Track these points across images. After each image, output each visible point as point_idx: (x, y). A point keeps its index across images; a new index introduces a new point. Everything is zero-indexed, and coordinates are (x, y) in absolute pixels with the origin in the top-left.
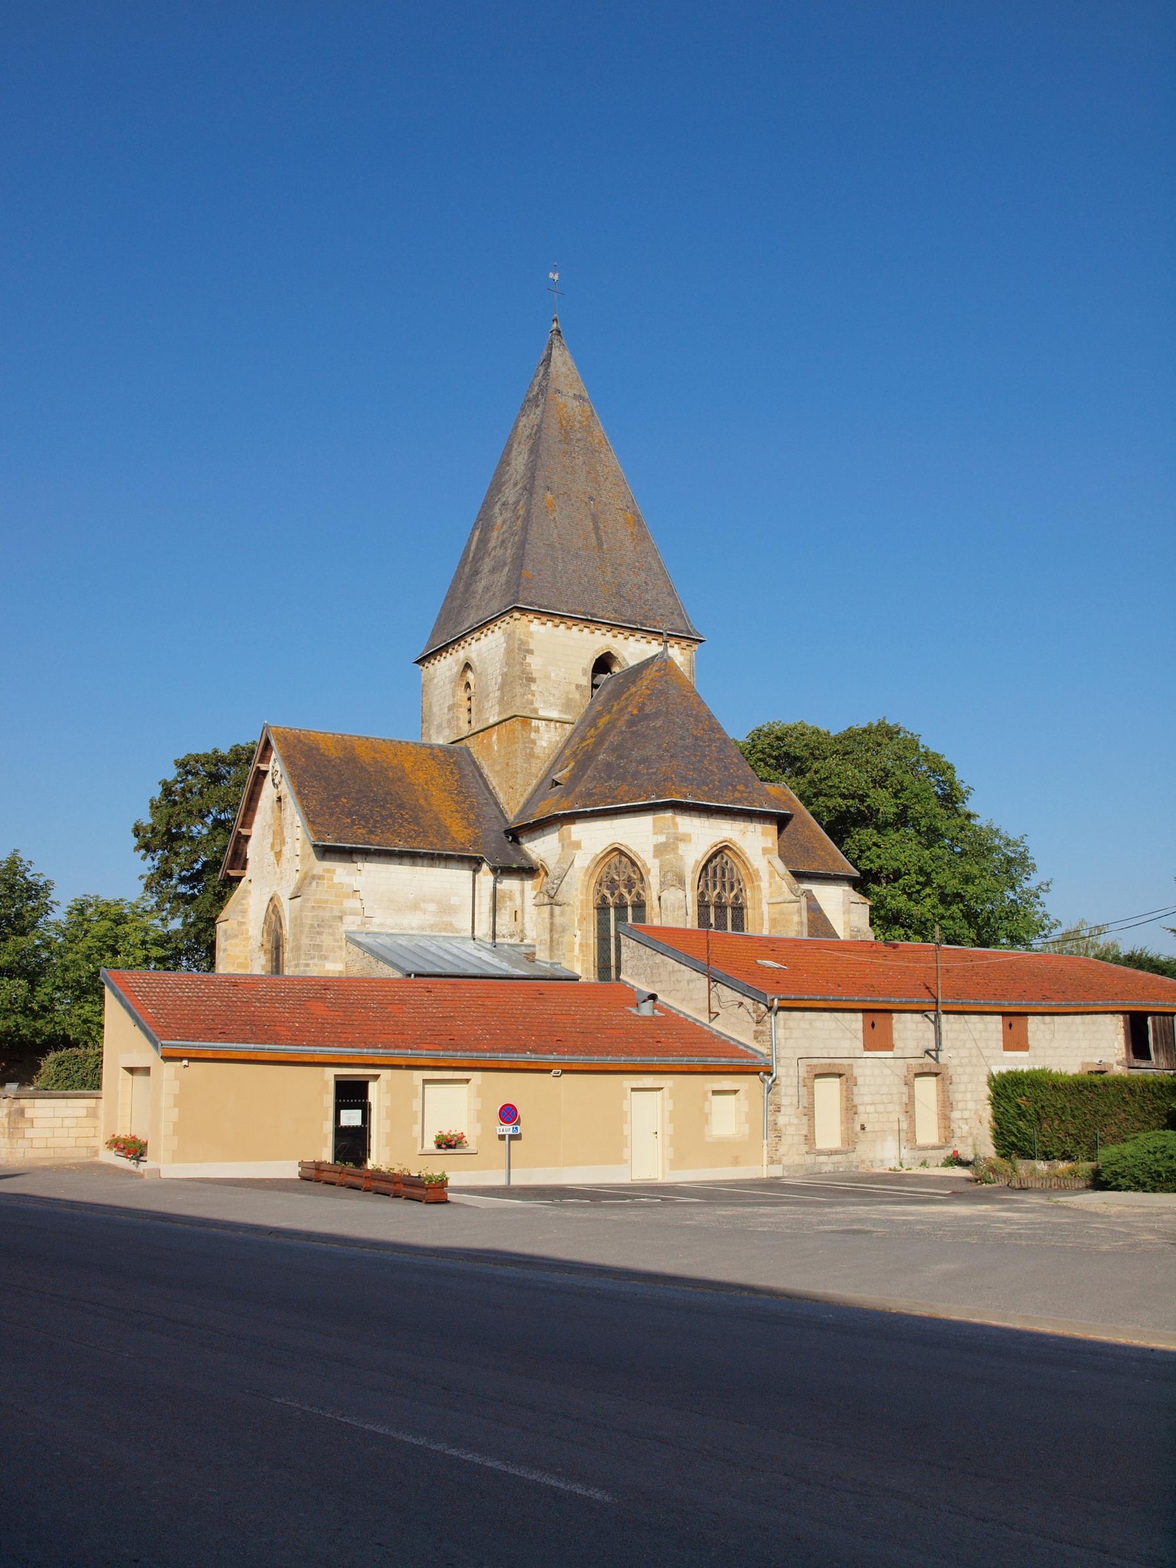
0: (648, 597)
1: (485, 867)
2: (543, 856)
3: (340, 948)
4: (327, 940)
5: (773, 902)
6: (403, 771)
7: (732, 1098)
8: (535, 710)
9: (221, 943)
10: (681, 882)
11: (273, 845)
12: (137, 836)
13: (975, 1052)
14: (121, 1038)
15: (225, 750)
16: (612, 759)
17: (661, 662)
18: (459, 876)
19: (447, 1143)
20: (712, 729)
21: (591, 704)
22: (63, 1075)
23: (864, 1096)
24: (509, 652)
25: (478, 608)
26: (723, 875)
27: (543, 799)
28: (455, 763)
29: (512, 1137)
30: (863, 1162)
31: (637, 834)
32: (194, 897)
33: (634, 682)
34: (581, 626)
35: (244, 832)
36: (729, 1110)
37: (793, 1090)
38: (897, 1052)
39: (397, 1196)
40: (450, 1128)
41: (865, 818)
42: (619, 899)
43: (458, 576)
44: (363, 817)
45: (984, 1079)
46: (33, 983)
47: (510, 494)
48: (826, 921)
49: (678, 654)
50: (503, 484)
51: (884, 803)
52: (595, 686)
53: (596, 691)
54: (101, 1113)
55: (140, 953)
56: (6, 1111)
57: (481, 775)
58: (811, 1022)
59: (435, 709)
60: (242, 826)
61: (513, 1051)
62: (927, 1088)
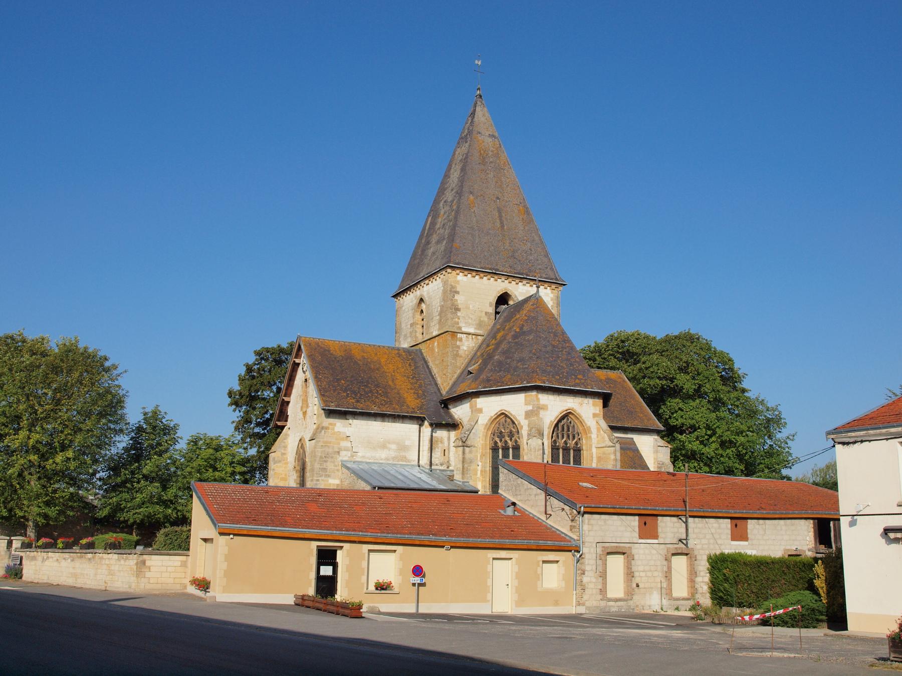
0: (531, 258)
1: (426, 423)
2: (461, 417)
3: (338, 470)
4: (330, 466)
5: (599, 447)
6: (380, 364)
7: (555, 565)
8: (460, 328)
9: (272, 465)
10: (541, 435)
11: (302, 408)
12: (230, 397)
13: (712, 541)
14: (201, 523)
15: (285, 345)
16: (502, 359)
17: (535, 300)
18: (413, 428)
19: (382, 587)
20: (564, 341)
21: (495, 324)
22: (168, 542)
23: (638, 566)
24: (445, 292)
25: (428, 265)
26: (568, 430)
27: (463, 382)
28: (412, 359)
29: (420, 585)
30: (637, 606)
31: (515, 404)
32: (264, 435)
33: (519, 312)
34: (489, 277)
35: (286, 399)
36: (553, 573)
37: (593, 562)
38: (661, 540)
39: (325, 611)
40: (384, 578)
41: (675, 392)
42: (504, 445)
43: (417, 248)
44: (354, 392)
45: (705, 558)
46: (164, 488)
47: (449, 196)
48: (641, 457)
49: (547, 295)
50: (445, 189)
51: (685, 381)
52: (497, 313)
53: (498, 316)
54: (189, 565)
55: (229, 470)
56: (135, 561)
57: (428, 367)
58: (605, 520)
59: (403, 325)
60: (285, 396)
61: (422, 534)
62: (680, 564)
